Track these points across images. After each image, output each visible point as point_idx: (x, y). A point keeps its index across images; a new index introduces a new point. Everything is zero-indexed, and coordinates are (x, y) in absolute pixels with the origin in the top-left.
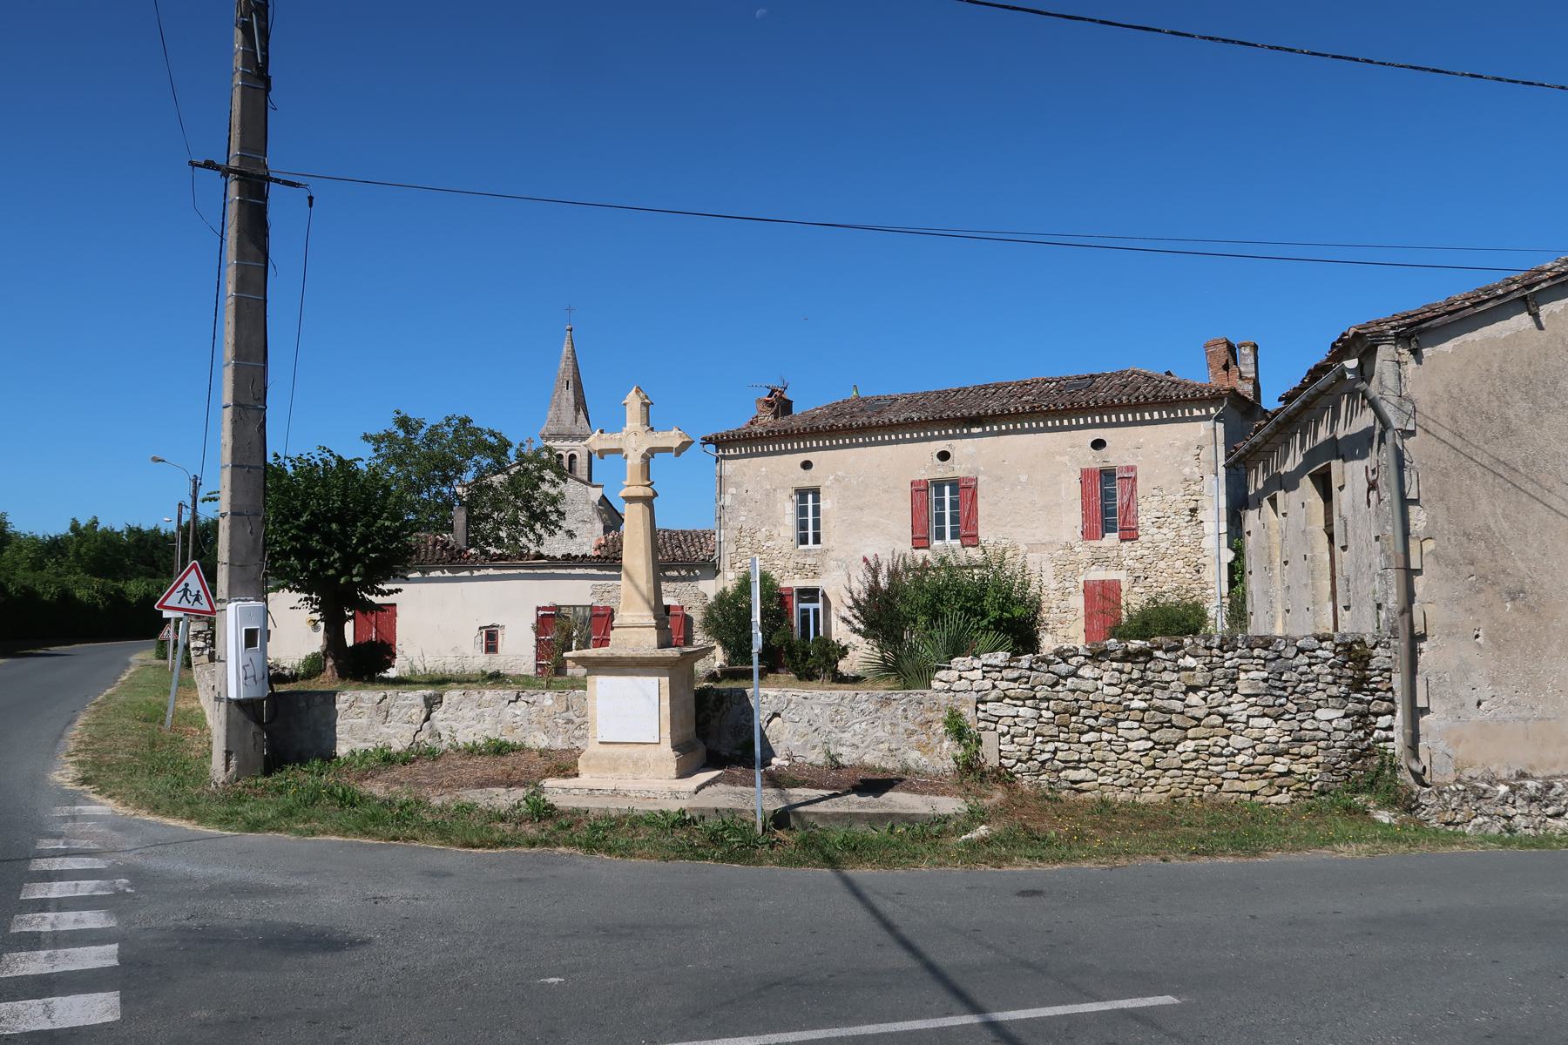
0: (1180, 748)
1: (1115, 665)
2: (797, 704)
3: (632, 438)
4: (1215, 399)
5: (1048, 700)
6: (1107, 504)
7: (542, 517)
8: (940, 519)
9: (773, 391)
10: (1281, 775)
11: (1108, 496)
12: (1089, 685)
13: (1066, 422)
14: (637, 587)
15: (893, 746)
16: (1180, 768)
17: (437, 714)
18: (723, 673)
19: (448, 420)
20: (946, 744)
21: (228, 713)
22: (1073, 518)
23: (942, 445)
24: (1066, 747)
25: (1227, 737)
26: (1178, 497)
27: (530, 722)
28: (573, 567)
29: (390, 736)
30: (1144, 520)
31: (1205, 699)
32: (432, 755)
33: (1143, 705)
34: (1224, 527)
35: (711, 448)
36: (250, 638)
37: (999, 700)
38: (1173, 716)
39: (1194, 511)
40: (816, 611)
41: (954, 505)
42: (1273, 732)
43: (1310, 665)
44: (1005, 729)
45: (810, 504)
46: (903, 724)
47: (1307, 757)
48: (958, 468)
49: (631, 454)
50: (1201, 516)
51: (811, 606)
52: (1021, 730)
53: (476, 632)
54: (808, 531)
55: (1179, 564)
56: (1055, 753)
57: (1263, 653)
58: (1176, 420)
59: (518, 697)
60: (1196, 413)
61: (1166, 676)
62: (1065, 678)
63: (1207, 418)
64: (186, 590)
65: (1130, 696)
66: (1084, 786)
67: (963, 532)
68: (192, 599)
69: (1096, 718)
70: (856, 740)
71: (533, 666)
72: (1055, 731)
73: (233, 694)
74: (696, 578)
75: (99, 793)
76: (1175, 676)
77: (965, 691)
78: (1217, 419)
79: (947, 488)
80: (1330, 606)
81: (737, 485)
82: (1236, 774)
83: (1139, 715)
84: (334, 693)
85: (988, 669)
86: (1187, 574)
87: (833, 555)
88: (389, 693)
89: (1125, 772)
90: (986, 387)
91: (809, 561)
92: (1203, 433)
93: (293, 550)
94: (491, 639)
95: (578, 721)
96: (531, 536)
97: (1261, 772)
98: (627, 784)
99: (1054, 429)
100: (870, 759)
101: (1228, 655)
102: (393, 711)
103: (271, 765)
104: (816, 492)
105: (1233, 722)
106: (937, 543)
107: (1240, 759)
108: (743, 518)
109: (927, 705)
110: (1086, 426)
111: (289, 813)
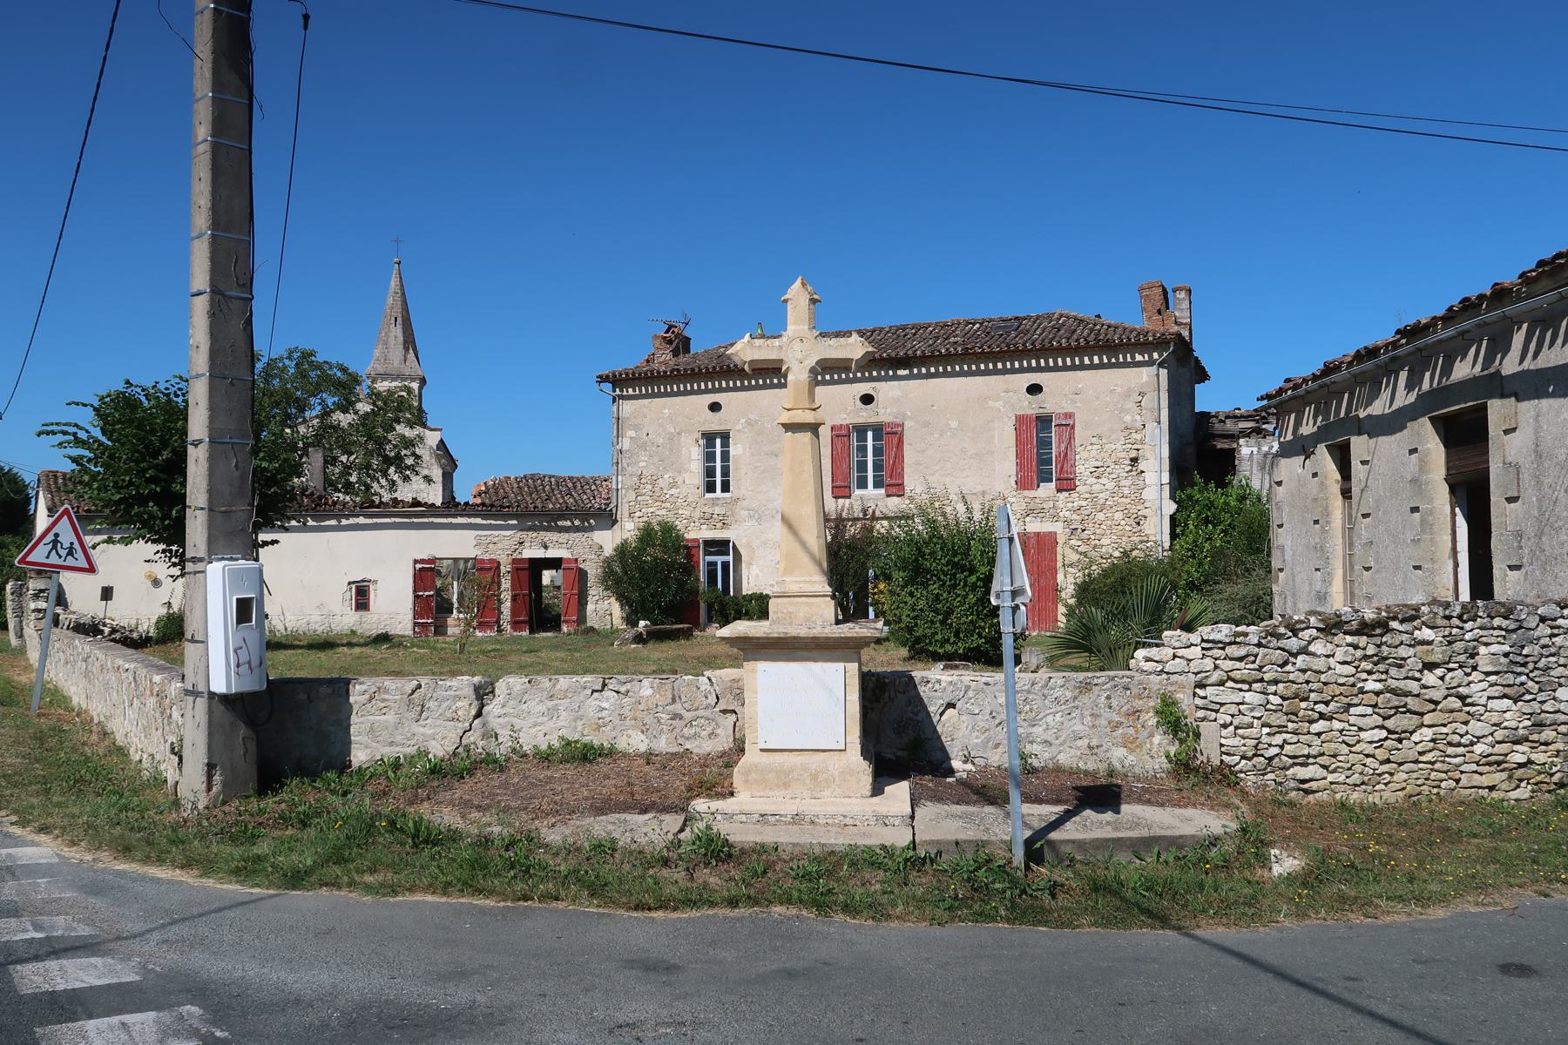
0: (1416, 737)
1: (1349, 639)
2: (977, 692)
3: (797, 346)
4: (1161, 343)
5: (1276, 682)
6: (1043, 452)
7: (398, 461)
8: (862, 466)
9: (670, 327)
10: (1521, 765)
11: (1045, 443)
12: (1319, 664)
13: (1000, 366)
14: (803, 544)
15: (1094, 743)
16: (1417, 762)
17: (492, 708)
18: (649, 633)
19: (291, 352)
20: (1157, 739)
21: (210, 712)
22: (1007, 467)
23: (865, 388)
24: (1295, 739)
25: (1466, 723)
26: (1118, 446)
27: (622, 717)
28: (455, 516)
29: (427, 738)
30: (1082, 469)
31: (1442, 678)
32: (491, 763)
33: (1379, 686)
34: (1166, 478)
35: (608, 387)
36: (244, 610)
37: (1222, 683)
38: (1409, 700)
39: (1134, 460)
40: (725, 566)
41: (878, 452)
42: (1512, 715)
43: (1552, 636)
44: (1229, 719)
45: (718, 450)
46: (1107, 714)
47: (1546, 744)
48: (882, 413)
49: (795, 367)
50: (1142, 466)
51: (719, 559)
52: (1247, 720)
53: (345, 587)
54: (716, 479)
55: (1118, 516)
56: (1282, 747)
57: (1505, 623)
58: (1118, 365)
59: (604, 685)
60: (1138, 358)
61: (1403, 652)
62: (1295, 655)
63: (1151, 363)
64: (55, 542)
65: (1364, 676)
66: (1314, 785)
67: (889, 481)
68: (63, 553)
69: (1327, 703)
70: (1049, 736)
71: (410, 625)
72: (1282, 720)
73: (219, 685)
74: (591, 529)
75: (23, 823)
76: (1411, 651)
77: (1180, 673)
78: (1161, 365)
79: (870, 434)
80: (1450, 564)
81: (636, 428)
82: (1474, 767)
83: (1373, 699)
84: (347, 682)
85: (1209, 645)
86: (1127, 525)
87: (745, 504)
88: (424, 681)
89: (1358, 768)
90: (904, 328)
91: (717, 510)
92: (1145, 379)
93: (152, 496)
94: (361, 595)
95: (688, 715)
96: (383, 482)
97: (1499, 763)
98: (808, 806)
99: (987, 373)
100: (1066, 758)
101: (1469, 625)
102: (431, 704)
103: (268, 780)
104: (725, 437)
105: (1472, 705)
106: (858, 492)
107: (1479, 748)
108: (643, 463)
109: (1135, 691)
110: (1022, 370)
111: (338, 857)
